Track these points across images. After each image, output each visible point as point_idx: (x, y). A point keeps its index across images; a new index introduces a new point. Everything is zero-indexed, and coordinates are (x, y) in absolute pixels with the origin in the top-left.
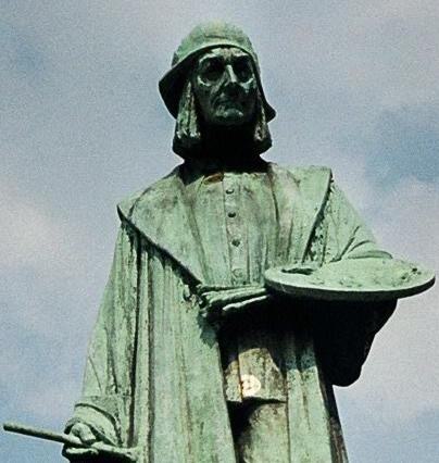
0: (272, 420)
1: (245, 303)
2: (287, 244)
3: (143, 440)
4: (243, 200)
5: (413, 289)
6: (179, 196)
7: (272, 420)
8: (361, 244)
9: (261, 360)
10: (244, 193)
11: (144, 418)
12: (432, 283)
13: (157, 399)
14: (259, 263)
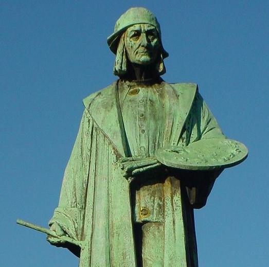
0: (156, 233)
1: (145, 168)
3: (88, 238)
4: (148, 107)
5: (239, 161)
7: (156, 233)
8: (211, 129)
9: (153, 198)
10: (149, 102)
12: (247, 156)
13: (96, 218)
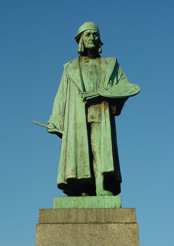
0: (98, 127)
1: (92, 97)
2: (104, 81)
3: (66, 130)
4: (94, 69)
6: (78, 66)
7: (98, 127)
8: (123, 79)
10: (94, 66)
11: (73, 109)
14: (97, 85)
